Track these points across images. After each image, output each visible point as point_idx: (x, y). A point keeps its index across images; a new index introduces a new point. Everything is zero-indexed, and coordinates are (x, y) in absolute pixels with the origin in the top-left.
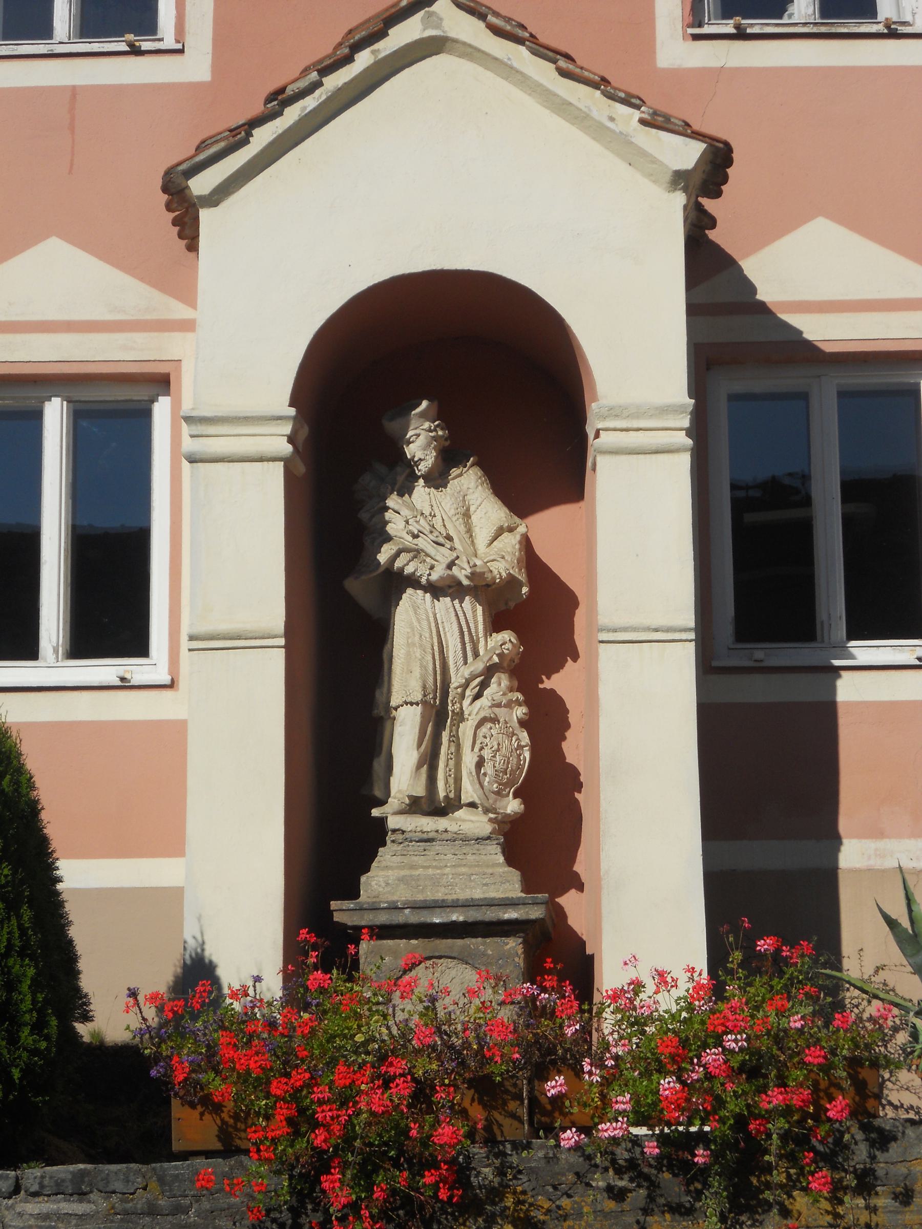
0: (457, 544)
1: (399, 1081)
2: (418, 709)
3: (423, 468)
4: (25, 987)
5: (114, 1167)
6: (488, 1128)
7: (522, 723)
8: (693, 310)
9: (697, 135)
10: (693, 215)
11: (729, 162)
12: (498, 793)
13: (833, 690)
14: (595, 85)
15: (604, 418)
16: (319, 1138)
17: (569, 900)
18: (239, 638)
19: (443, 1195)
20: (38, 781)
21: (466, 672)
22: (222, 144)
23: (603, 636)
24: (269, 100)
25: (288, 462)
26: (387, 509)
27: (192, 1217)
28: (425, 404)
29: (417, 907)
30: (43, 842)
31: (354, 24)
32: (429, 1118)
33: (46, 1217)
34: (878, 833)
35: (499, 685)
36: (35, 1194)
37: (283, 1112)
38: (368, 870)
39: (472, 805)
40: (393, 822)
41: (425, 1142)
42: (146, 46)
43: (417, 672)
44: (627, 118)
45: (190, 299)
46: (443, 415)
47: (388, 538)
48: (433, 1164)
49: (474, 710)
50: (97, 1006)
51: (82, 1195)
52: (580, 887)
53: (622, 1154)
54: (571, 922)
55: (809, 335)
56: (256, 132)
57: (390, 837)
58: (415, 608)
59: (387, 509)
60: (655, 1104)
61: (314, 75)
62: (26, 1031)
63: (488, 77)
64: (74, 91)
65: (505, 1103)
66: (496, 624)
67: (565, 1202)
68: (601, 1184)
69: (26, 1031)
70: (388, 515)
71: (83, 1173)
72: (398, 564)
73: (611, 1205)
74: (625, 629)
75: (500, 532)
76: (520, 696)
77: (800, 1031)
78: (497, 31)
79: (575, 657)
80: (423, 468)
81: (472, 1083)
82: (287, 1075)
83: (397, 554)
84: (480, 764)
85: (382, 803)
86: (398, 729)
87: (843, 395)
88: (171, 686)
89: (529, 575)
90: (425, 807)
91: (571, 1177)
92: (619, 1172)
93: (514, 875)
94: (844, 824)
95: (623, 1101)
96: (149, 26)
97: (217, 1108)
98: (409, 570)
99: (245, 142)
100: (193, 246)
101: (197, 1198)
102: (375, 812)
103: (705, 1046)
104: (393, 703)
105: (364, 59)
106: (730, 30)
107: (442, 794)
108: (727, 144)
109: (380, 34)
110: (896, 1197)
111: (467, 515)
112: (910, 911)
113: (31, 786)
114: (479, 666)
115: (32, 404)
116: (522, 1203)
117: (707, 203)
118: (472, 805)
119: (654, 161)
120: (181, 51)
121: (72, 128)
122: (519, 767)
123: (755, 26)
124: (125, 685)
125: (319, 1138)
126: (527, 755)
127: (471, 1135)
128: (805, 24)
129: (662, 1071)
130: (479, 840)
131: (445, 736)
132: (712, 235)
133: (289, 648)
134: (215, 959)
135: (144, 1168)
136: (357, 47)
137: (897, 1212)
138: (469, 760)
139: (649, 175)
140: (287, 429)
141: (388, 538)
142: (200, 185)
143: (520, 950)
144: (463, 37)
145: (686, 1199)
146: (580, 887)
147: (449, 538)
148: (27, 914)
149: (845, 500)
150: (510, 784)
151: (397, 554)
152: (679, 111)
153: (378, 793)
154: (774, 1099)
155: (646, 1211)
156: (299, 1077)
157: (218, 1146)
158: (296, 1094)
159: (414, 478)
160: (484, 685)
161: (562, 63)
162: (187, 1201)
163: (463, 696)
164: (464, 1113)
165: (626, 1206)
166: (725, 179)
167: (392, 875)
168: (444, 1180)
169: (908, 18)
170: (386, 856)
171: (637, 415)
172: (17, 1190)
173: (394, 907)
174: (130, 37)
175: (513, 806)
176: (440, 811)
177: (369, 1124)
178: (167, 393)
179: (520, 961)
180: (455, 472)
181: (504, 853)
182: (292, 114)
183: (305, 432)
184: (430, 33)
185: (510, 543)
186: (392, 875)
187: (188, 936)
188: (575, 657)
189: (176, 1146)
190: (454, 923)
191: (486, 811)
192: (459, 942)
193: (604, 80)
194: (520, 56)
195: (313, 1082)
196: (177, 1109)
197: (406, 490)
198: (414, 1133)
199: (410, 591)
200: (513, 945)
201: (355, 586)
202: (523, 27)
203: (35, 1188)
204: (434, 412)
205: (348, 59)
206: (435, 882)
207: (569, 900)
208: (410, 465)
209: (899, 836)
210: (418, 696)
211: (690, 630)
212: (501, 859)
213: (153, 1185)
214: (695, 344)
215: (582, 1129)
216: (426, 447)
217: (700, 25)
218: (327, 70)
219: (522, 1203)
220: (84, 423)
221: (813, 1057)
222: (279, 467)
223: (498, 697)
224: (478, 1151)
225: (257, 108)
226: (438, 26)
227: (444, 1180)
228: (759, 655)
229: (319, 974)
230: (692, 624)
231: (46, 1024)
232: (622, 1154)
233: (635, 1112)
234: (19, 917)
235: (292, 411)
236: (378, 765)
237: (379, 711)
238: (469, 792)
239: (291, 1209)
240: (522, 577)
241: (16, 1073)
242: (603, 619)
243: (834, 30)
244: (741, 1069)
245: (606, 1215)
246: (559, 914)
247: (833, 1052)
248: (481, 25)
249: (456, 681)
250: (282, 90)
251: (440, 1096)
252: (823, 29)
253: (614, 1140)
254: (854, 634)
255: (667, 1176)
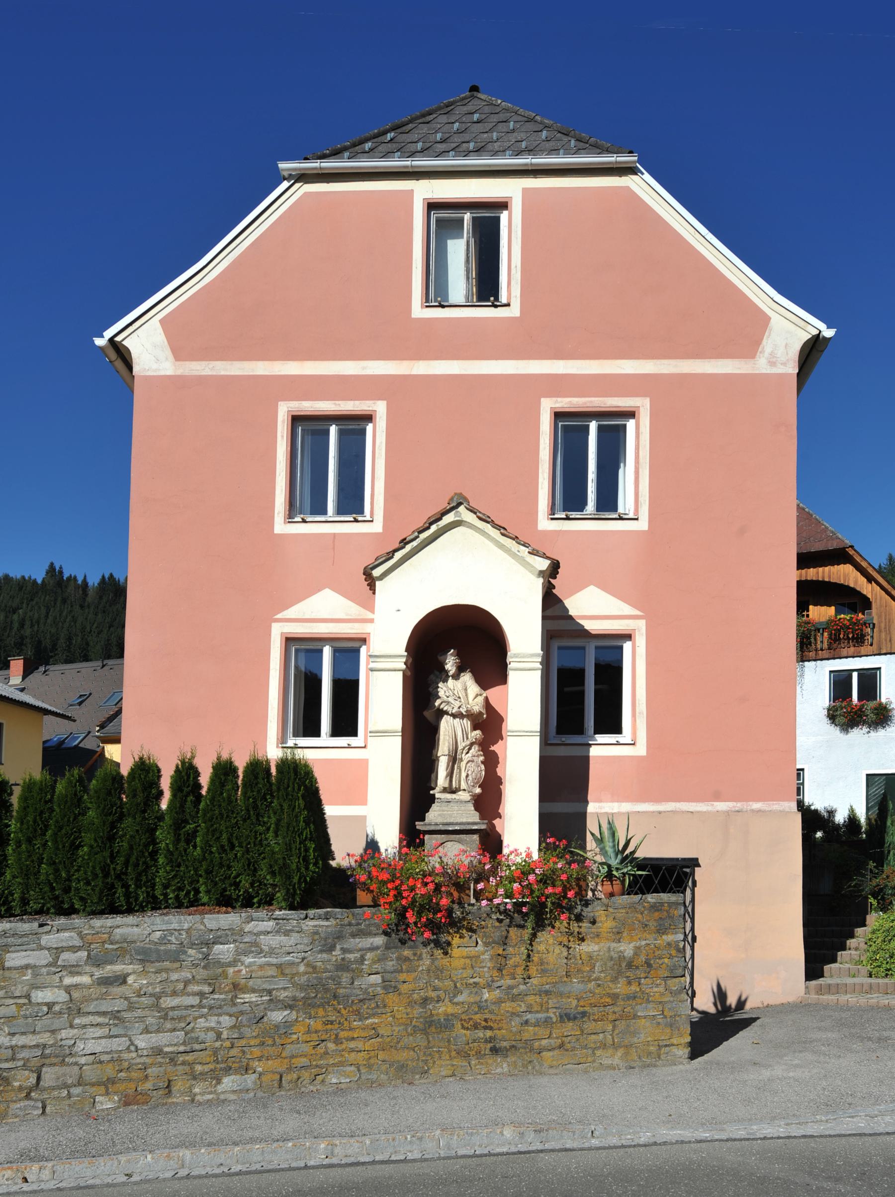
0: (462, 700)
1: (431, 884)
2: (447, 757)
3: (451, 673)
4: (311, 851)
5: (338, 910)
6: (459, 899)
7: (482, 762)
8: (544, 618)
9: (548, 558)
10: (547, 584)
11: (559, 567)
12: (473, 786)
13: (588, 751)
14: (514, 539)
15: (512, 658)
16: (404, 902)
17: (496, 822)
18: (386, 732)
19: (443, 920)
20: (318, 780)
21: (464, 744)
22: (384, 558)
23: (509, 734)
24: (400, 543)
25: (404, 672)
26: (438, 687)
27: (363, 926)
28: (452, 651)
29: (444, 824)
30: (320, 801)
31: (430, 516)
32: (439, 896)
33: (316, 926)
34: (600, 801)
35: (475, 749)
36: (312, 919)
37: (392, 893)
38: (428, 811)
39: (464, 790)
40: (437, 796)
41: (438, 904)
42: (360, 519)
43: (447, 744)
44: (524, 551)
45: (372, 610)
46: (459, 655)
47: (439, 697)
48: (440, 911)
49: (466, 758)
50: (336, 855)
51: (327, 919)
52: (500, 817)
53: (502, 908)
54: (497, 829)
55: (587, 627)
56: (396, 554)
57: (436, 801)
58: (447, 722)
59: (438, 687)
60: (512, 892)
61: (416, 534)
62: (312, 865)
63: (477, 535)
64: (334, 535)
65: (465, 891)
66: (475, 728)
67: (483, 923)
68: (495, 917)
69: (312, 865)
70: (439, 689)
71: (328, 912)
72: (442, 707)
73: (497, 924)
74: (516, 732)
75: (477, 696)
76: (482, 753)
77: (561, 869)
78: (480, 519)
79: (502, 739)
80: (451, 673)
81: (454, 884)
82: (394, 882)
83: (441, 703)
84: (467, 776)
85: (434, 789)
86: (440, 764)
87: (597, 648)
88: (365, 747)
89: (487, 711)
90: (448, 790)
91: (485, 915)
92: (501, 914)
93: (477, 814)
94: (589, 798)
95: (501, 891)
96: (361, 511)
97: (372, 891)
98: (445, 709)
99: (392, 557)
100: (374, 593)
101: (365, 920)
102: (431, 792)
103: (530, 873)
104: (439, 755)
105: (434, 528)
106: (564, 516)
107: (454, 786)
108: (558, 561)
109: (440, 519)
110: (591, 923)
111: (466, 690)
112: (600, 830)
113: (316, 783)
114: (468, 742)
115: (320, 647)
116: (469, 923)
117: (552, 581)
118: (464, 790)
119: (533, 567)
120: (372, 521)
121: (334, 548)
122: (481, 777)
123: (573, 515)
124: (349, 747)
125: (404, 902)
126: (483, 773)
127: (453, 902)
128: (590, 514)
129: (515, 882)
130: (466, 802)
131: (456, 766)
132: (554, 591)
133: (402, 736)
134: (378, 840)
135: (347, 911)
136: (431, 524)
137: (590, 928)
138: (464, 775)
139: (531, 572)
140: (404, 660)
141: (439, 697)
142: (376, 573)
143: (478, 839)
144: (468, 520)
145: (522, 922)
146: (500, 817)
147: (459, 698)
148: (312, 826)
149: (596, 684)
150: (477, 783)
151: (441, 703)
152: (542, 550)
153: (433, 785)
154: (550, 890)
155: (509, 926)
156: (398, 882)
157: (372, 904)
158: (396, 888)
159: (448, 676)
160: (470, 749)
161: (502, 531)
162: (361, 921)
163: (462, 753)
164: (451, 894)
165: (502, 925)
166: (558, 573)
167: (436, 813)
168: (444, 916)
169: (627, 512)
170: (435, 807)
171: (523, 657)
172: (306, 917)
173: (436, 824)
174: (354, 515)
175: (478, 790)
176: (453, 792)
177: (420, 898)
178: (365, 644)
179: (478, 842)
180: (462, 674)
181: (474, 806)
182: (408, 548)
183: (411, 660)
184: (457, 519)
185: (480, 699)
186: (436, 813)
187: (369, 832)
188: (502, 739)
189: (358, 904)
190: (456, 830)
191: (469, 792)
192: (458, 836)
193: (516, 537)
194: (488, 528)
195: (402, 883)
196: (359, 892)
197: (445, 681)
198: (434, 901)
199: (445, 716)
200: (476, 837)
201: (428, 714)
202: (489, 517)
203: (312, 917)
204: (455, 653)
205: (428, 528)
206: (451, 816)
207: (496, 822)
208: (447, 672)
209: (607, 802)
210: (447, 753)
211: (806, 576)
212: (473, 808)
213: (350, 916)
214: (547, 631)
215: (488, 900)
216: (452, 666)
217: (554, 515)
218: (420, 532)
219: (469, 923)
220: (337, 654)
221: (564, 877)
222: (401, 673)
223: (474, 753)
224: (456, 906)
225: (397, 545)
226: (460, 516)
227: (444, 916)
228: (563, 739)
229: (405, 849)
230: (539, 730)
231: (318, 863)
232: (502, 908)
233: (505, 894)
234: (310, 828)
235: (406, 654)
236: (433, 776)
237: (434, 758)
238: (463, 785)
239: (395, 924)
240: (484, 711)
241: (308, 879)
242: (509, 728)
243: (600, 517)
244: (541, 881)
245: (496, 927)
246: (494, 826)
247: (571, 876)
248: (475, 516)
249: (460, 747)
250: (405, 539)
251: (443, 889)
252: (597, 517)
253: (499, 904)
254: (597, 731)
255: (516, 915)
